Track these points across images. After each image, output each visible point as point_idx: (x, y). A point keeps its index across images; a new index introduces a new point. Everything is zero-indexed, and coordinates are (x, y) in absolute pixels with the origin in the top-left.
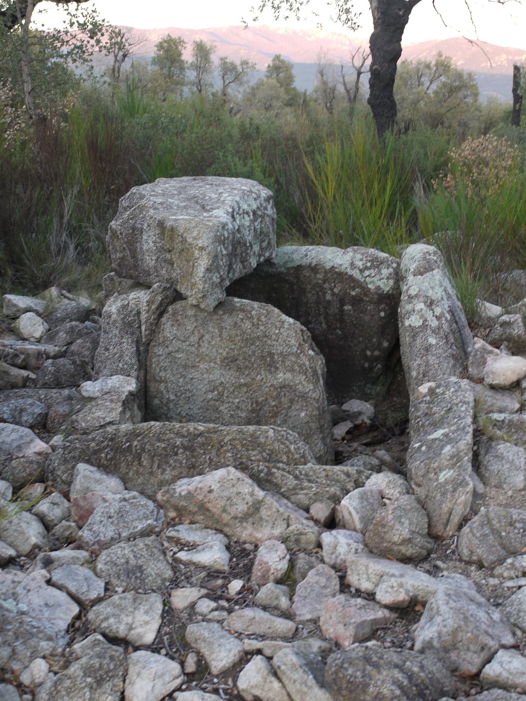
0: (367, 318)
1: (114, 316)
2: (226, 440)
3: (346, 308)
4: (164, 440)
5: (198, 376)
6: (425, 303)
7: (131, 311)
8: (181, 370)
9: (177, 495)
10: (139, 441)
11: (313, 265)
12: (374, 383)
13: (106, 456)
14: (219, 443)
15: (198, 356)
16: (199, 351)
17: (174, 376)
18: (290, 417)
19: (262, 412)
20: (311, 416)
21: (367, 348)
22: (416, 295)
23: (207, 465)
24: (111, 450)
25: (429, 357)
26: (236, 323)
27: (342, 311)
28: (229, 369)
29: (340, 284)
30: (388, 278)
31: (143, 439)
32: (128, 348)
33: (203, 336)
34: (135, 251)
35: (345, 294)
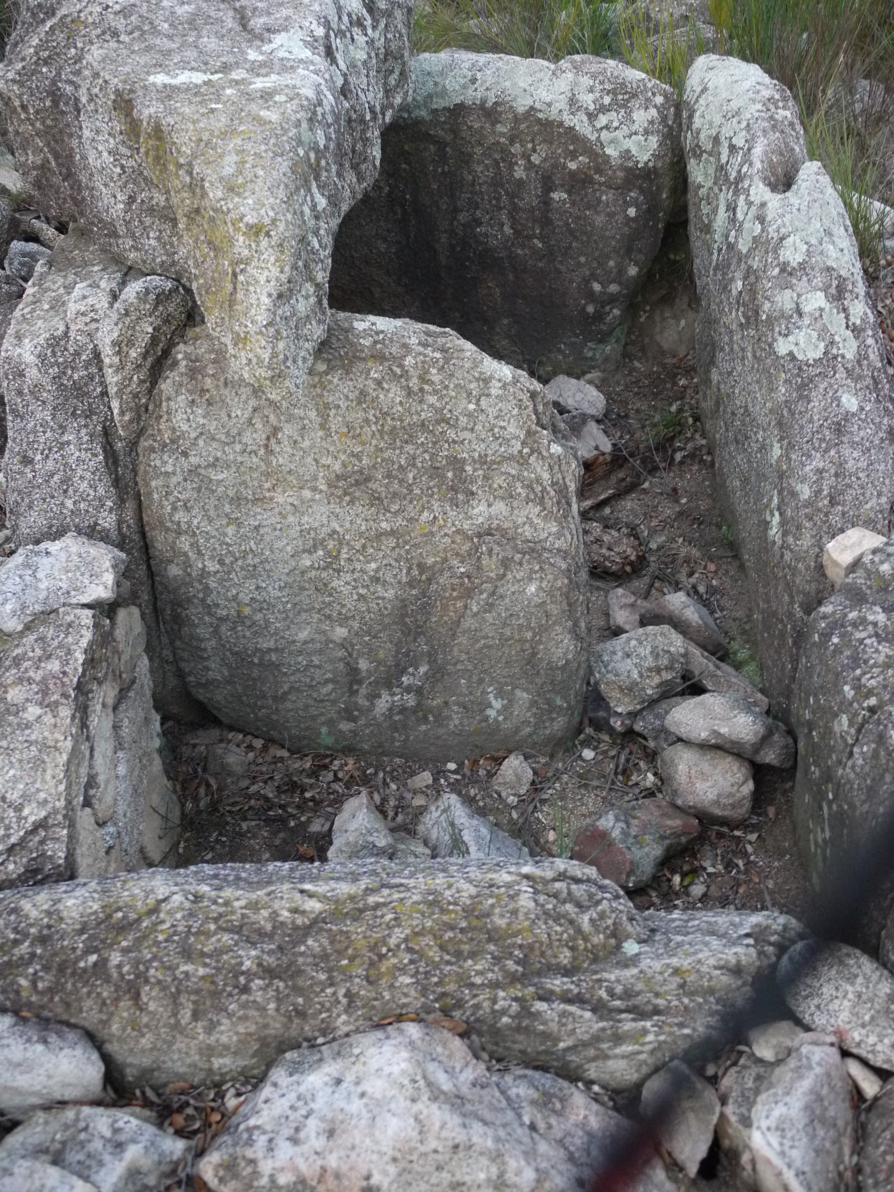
0: (599, 220)
1: (33, 374)
2: (393, 941)
3: (555, 196)
4: (203, 954)
5: (273, 520)
6: (826, 289)
7: (77, 354)
8: (227, 508)
9: (264, 1181)
10: (125, 951)
11: (489, 104)
12: (601, 341)
13: (34, 983)
14: (373, 948)
15: (268, 475)
16: (269, 464)
17: (210, 522)
18: (502, 597)
19: (434, 587)
20: (550, 593)
21: (594, 277)
22: (802, 266)
23: (341, 1008)
24: (46, 968)
25: (846, 450)
26: (363, 393)
27: (546, 202)
28: (352, 502)
29: (545, 146)
30: (647, 132)
31: (138, 941)
32: (83, 459)
33: (276, 430)
34: (71, 157)
35: (555, 166)
